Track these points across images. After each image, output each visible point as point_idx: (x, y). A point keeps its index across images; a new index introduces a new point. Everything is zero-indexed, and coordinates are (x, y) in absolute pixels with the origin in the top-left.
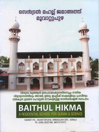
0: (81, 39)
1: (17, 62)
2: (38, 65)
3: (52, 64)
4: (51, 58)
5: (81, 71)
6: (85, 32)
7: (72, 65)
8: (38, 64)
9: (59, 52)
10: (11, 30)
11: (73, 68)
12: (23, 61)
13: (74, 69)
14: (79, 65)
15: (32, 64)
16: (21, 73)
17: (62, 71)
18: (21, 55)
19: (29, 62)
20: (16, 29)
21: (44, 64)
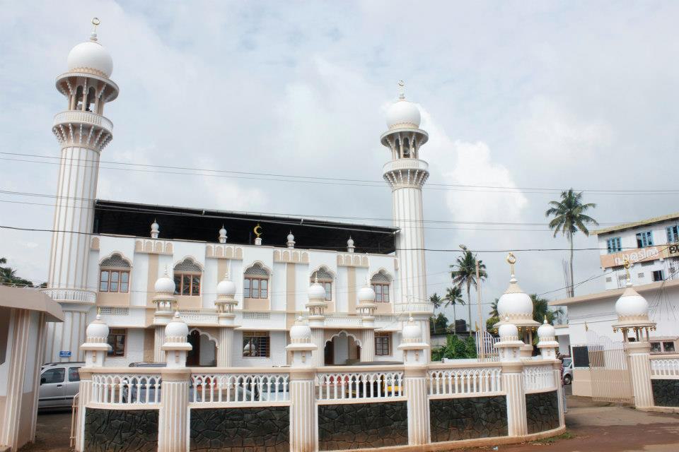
0: (65, 130)
1: (95, 250)
2: (196, 273)
3: (126, 263)
4: (264, 243)
5: (196, 308)
6: (411, 143)
7: (221, 277)
8: (198, 268)
9: (200, 212)
10: (390, 140)
11: (225, 286)
12: (123, 245)
13: (232, 296)
14: (381, 280)
15: (238, 271)
16: (111, 308)
17: (318, 308)
18: (114, 218)
19: (222, 260)
20: (411, 134)
21: (225, 269)
